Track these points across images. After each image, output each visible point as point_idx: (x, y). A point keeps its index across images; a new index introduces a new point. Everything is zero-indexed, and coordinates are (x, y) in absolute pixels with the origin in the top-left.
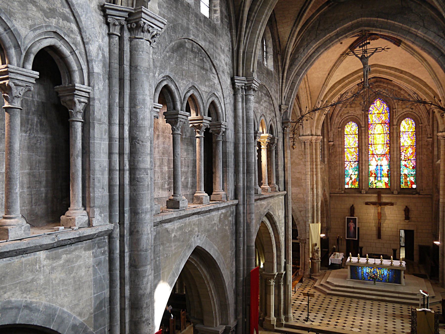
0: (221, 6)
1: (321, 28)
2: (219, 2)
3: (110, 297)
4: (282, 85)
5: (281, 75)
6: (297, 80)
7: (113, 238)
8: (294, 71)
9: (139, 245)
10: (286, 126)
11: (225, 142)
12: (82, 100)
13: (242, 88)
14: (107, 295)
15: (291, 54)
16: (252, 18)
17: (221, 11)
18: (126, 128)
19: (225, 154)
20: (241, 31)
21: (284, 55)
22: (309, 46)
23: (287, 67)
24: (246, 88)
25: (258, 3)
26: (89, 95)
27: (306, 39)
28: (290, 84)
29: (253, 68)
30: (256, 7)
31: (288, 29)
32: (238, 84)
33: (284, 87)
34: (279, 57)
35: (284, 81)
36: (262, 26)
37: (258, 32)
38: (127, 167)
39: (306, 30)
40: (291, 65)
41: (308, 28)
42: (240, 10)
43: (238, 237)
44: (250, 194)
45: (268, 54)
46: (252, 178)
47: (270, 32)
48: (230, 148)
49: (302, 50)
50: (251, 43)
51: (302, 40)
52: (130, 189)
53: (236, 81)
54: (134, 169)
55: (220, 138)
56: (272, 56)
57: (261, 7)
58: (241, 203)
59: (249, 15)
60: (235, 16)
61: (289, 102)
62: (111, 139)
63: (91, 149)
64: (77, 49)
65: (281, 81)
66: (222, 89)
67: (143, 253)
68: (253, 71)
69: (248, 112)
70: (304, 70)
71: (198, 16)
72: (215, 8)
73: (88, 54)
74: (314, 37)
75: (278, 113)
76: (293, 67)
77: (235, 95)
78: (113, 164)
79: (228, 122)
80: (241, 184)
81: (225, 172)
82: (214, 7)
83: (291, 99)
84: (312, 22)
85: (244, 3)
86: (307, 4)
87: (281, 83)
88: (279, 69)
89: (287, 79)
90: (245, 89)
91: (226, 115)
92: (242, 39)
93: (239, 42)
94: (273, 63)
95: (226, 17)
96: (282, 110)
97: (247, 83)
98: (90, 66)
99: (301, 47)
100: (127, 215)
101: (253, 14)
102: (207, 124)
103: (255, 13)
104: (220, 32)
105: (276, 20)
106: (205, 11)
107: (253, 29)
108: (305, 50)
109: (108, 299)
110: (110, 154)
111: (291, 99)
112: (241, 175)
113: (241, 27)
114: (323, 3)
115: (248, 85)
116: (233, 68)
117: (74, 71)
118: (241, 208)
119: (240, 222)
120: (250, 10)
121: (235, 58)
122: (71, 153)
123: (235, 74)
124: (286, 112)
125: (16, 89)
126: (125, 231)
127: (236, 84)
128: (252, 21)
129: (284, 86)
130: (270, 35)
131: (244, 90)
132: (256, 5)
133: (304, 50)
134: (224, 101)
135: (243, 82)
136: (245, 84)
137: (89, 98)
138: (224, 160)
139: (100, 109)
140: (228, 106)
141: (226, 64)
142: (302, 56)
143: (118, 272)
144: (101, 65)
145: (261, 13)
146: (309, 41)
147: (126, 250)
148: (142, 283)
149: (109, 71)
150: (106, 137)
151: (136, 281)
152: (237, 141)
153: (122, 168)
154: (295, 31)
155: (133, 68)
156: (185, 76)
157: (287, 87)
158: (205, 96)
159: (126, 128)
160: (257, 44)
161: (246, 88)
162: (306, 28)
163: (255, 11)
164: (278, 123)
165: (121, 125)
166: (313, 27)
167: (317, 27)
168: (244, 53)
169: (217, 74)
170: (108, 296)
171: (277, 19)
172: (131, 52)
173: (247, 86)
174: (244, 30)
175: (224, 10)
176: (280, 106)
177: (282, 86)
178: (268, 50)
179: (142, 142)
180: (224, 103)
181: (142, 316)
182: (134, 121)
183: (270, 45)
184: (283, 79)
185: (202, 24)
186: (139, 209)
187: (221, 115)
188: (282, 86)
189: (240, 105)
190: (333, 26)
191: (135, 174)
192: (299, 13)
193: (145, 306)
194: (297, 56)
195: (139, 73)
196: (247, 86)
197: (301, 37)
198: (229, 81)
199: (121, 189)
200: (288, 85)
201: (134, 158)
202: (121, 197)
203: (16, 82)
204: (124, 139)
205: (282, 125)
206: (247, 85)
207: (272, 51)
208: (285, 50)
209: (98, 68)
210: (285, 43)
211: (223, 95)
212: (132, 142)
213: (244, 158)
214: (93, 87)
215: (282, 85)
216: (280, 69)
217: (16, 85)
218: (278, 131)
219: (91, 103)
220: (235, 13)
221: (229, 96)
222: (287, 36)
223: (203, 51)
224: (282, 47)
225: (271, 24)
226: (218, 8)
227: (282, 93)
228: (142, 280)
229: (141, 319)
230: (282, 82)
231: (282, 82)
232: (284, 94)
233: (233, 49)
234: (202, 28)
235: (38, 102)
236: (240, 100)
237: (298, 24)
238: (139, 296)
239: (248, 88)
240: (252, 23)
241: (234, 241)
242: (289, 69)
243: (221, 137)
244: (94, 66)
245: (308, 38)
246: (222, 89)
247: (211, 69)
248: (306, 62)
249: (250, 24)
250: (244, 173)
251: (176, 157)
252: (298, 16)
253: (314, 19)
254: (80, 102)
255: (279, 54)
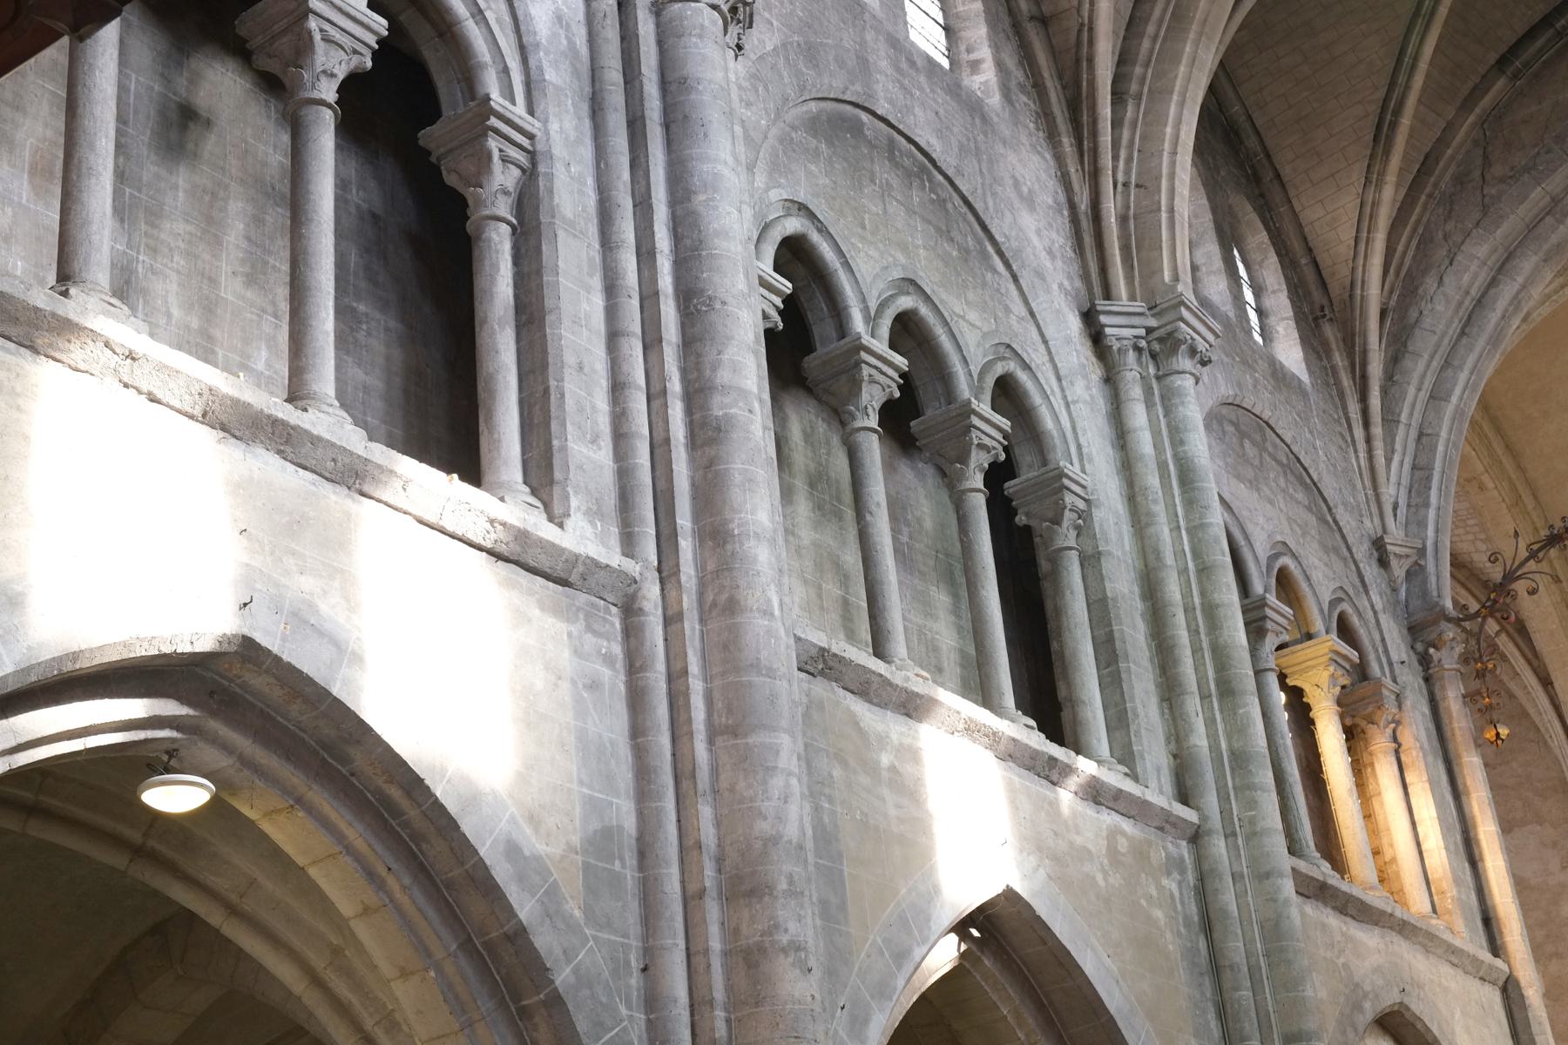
0: (996, 48)
1: (1497, 170)
2: (979, 6)
3: (640, 838)
4: (1370, 451)
5: (1354, 408)
6: (1441, 419)
7: (641, 611)
8: (1415, 381)
9: (740, 650)
10: (1433, 636)
11: (1091, 560)
12: (513, 153)
13: (1138, 349)
14: (630, 824)
15: (1383, 314)
16: (1134, 87)
17: (999, 65)
18: (665, 265)
19: (1100, 609)
20: (1094, 134)
21: (1353, 319)
22: (1459, 258)
23: (1376, 369)
24: (1156, 347)
25: (1151, 29)
26: (533, 145)
27: (1440, 234)
28: (1411, 445)
29: (1175, 269)
30: (1146, 44)
31: (1347, 204)
32: (1118, 331)
33: (1380, 460)
34: (1329, 331)
35: (1377, 430)
36: (1182, 104)
37: (1169, 130)
38: (675, 385)
39: (1430, 196)
40: (1394, 361)
41: (1436, 185)
42: (1078, 61)
43: (1227, 985)
44: (1251, 787)
45: (1272, 320)
46: (1247, 715)
47: (1261, 226)
48: (1122, 584)
49: (1430, 283)
50: (1148, 185)
51: (1425, 243)
52: (692, 460)
53: (1103, 319)
54: (701, 390)
55: (1066, 536)
56: (1292, 323)
57: (1165, 39)
58: (1216, 821)
59: (1119, 80)
60: (1064, 88)
61: (1422, 524)
62: (611, 289)
63: (549, 303)
64: (489, 8)
65: (1359, 433)
66: (1045, 342)
67: (756, 679)
68: (1176, 279)
69: (1182, 442)
70: (1461, 368)
71: (900, 46)
72: (973, 57)
73: (523, 28)
74: (1477, 216)
75: (1371, 571)
76: (1407, 363)
77: (1111, 380)
78: (625, 368)
79: (1091, 468)
80: (1199, 739)
81: (1112, 680)
82: (969, 51)
83: (1432, 514)
84: (1452, 158)
85: (1091, 29)
86: (1401, 79)
87: (1361, 446)
88: (1338, 383)
89: (1390, 421)
90: (1154, 356)
91: (1079, 447)
92: (1106, 160)
93: (1094, 176)
94: (1299, 348)
95: (1022, 87)
96: (1394, 562)
97: (1153, 323)
98: (532, 63)
99: (1425, 273)
100: (686, 545)
101: (1138, 70)
102: (995, 444)
103: (1147, 65)
104: (1005, 130)
105: (1278, 176)
106: (926, 35)
107: (1145, 123)
108: (1446, 279)
109: (633, 842)
110: (614, 337)
111: (1432, 514)
112: (1193, 704)
113: (1094, 121)
114: (1482, 70)
115: (1161, 333)
116: (1085, 277)
117: (482, 66)
118: (1218, 847)
119: (1225, 913)
120: (1124, 60)
121: (1088, 240)
122: (479, 315)
123: (1097, 290)
124: (1416, 573)
125: (326, 54)
126: (685, 598)
127: (1108, 331)
128: (1139, 97)
129: (1379, 453)
130: (1263, 236)
131: (1146, 357)
132: (1141, 35)
133: (1441, 281)
134: (1063, 390)
135: (1136, 321)
136: (1149, 330)
137: (532, 154)
138: (1101, 632)
139: (571, 193)
140: (1081, 411)
141: (1050, 253)
142: (1439, 308)
143: (664, 740)
144: (565, 66)
145: (1169, 57)
146: (1458, 238)
147: (694, 667)
148: (765, 791)
149: (594, 93)
150: (597, 282)
151: (742, 785)
152: (1151, 557)
153: (656, 387)
154: (1375, 204)
155: (673, 88)
156: (873, 234)
157: (1396, 458)
158: (970, 339)
159: (665, 265)
160: (1172, 176)
161: (1156, 347)
162: (1428, 190)
163: (1141, 57)
164: (1383, 618)
165: (646, 254)
166: (1460, 180)
167: (1477, 174)
168: (1123, 220)
169: (1015, 278)
170: (633, 832)
171: (1286, 172)
172: (660, 43)
173: (1160, 340)
174: (1106, 138)
175: (1011, 62)
176: (1379, 545)
177: (1371, 457)
178: (1269, 302)
179: (724, 303)
180: (1065, 397)
181: (776, 926)
182: (688, 242)
183: (1272, 275)
184: (1367, 424)
185: (922, 79)
186: (732, 521)
187: (1057, 441)
188: (1371, 457)
189: (1138, 416)
190: (1548, 152)
191: (705, 407)
192: (1379, 127)
193: (783, 886)
194: (1413, 314)
195: (693, 96)
196: (1160, 340)
197: (1414, 230)
198: (1074, 324)
199: (657, 458)
200: (1398, 447)
201: (699, 355)
202: (662, 485)
203: (327, 27)
204: (657, 293)
205: (1414, 640)
206: (1156, 334)
207: (1287, 303)
208: (1351, 296)
209: (555, 74)
210: (1345, 271)
211: (1055, 367)
212: (687, 307)
213: (1194, 632)
214: (546, 122)
215: (1370, 451)
216: (1346, 382)
217: (327, 40)
218: (1395, 657)
219: (541, 168)
220: (1060, 78)
221: (1085, 377)
222: (1347, 234)
223: (940, 178)
224: (1335, 289)
225: (1262, 195)
226: (985, 53)
227: (1375, 487)
228: (765, 782)
229: (771, 935)
230: (1368, 440)
231: (1368, 440)
232: (1392, 490)
233: (1072, 206)
234: (921, 89)
235: (358, 207)
236: (1136, 392)
237: (1382, 174)
238: (758, 845)
239: (1162, 346)
240: (1139, 105)
241: (1211, 1016)
242: (1389, 378)
243: (1073, 534)
244: (545, 64)
245: (1450, 226)
246: (1045, 342)
247: (984, 256)
248: (1463, 333)
249: (1130, 108)
250: (1205, 697)
251: (868, 517)
252: (1376, 139)
253: (1455, 143)
254: (505, 160)
255: (1322, 309)
